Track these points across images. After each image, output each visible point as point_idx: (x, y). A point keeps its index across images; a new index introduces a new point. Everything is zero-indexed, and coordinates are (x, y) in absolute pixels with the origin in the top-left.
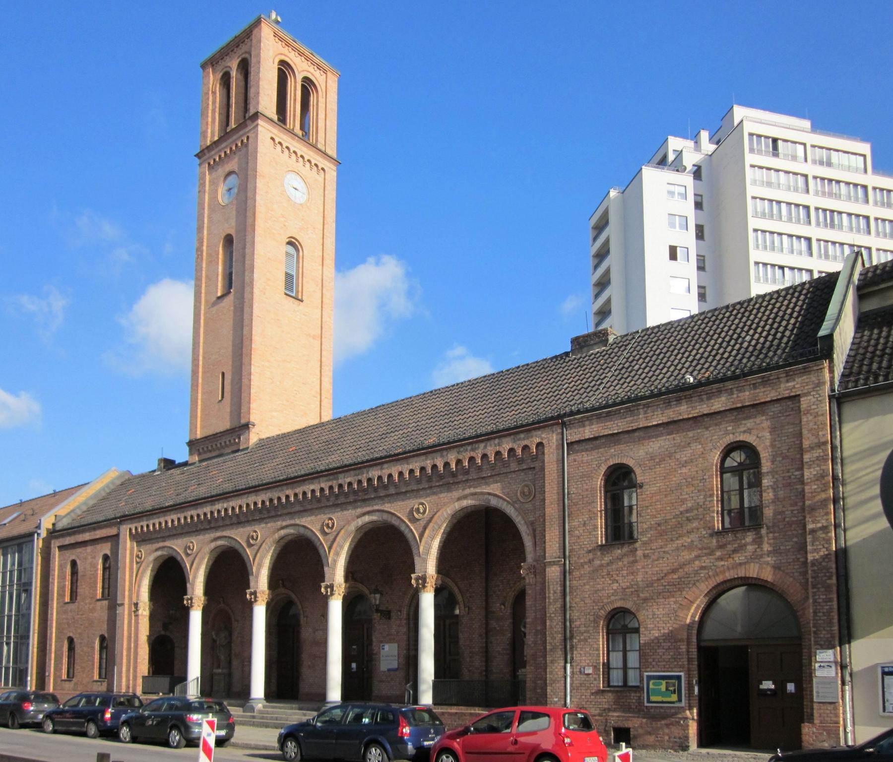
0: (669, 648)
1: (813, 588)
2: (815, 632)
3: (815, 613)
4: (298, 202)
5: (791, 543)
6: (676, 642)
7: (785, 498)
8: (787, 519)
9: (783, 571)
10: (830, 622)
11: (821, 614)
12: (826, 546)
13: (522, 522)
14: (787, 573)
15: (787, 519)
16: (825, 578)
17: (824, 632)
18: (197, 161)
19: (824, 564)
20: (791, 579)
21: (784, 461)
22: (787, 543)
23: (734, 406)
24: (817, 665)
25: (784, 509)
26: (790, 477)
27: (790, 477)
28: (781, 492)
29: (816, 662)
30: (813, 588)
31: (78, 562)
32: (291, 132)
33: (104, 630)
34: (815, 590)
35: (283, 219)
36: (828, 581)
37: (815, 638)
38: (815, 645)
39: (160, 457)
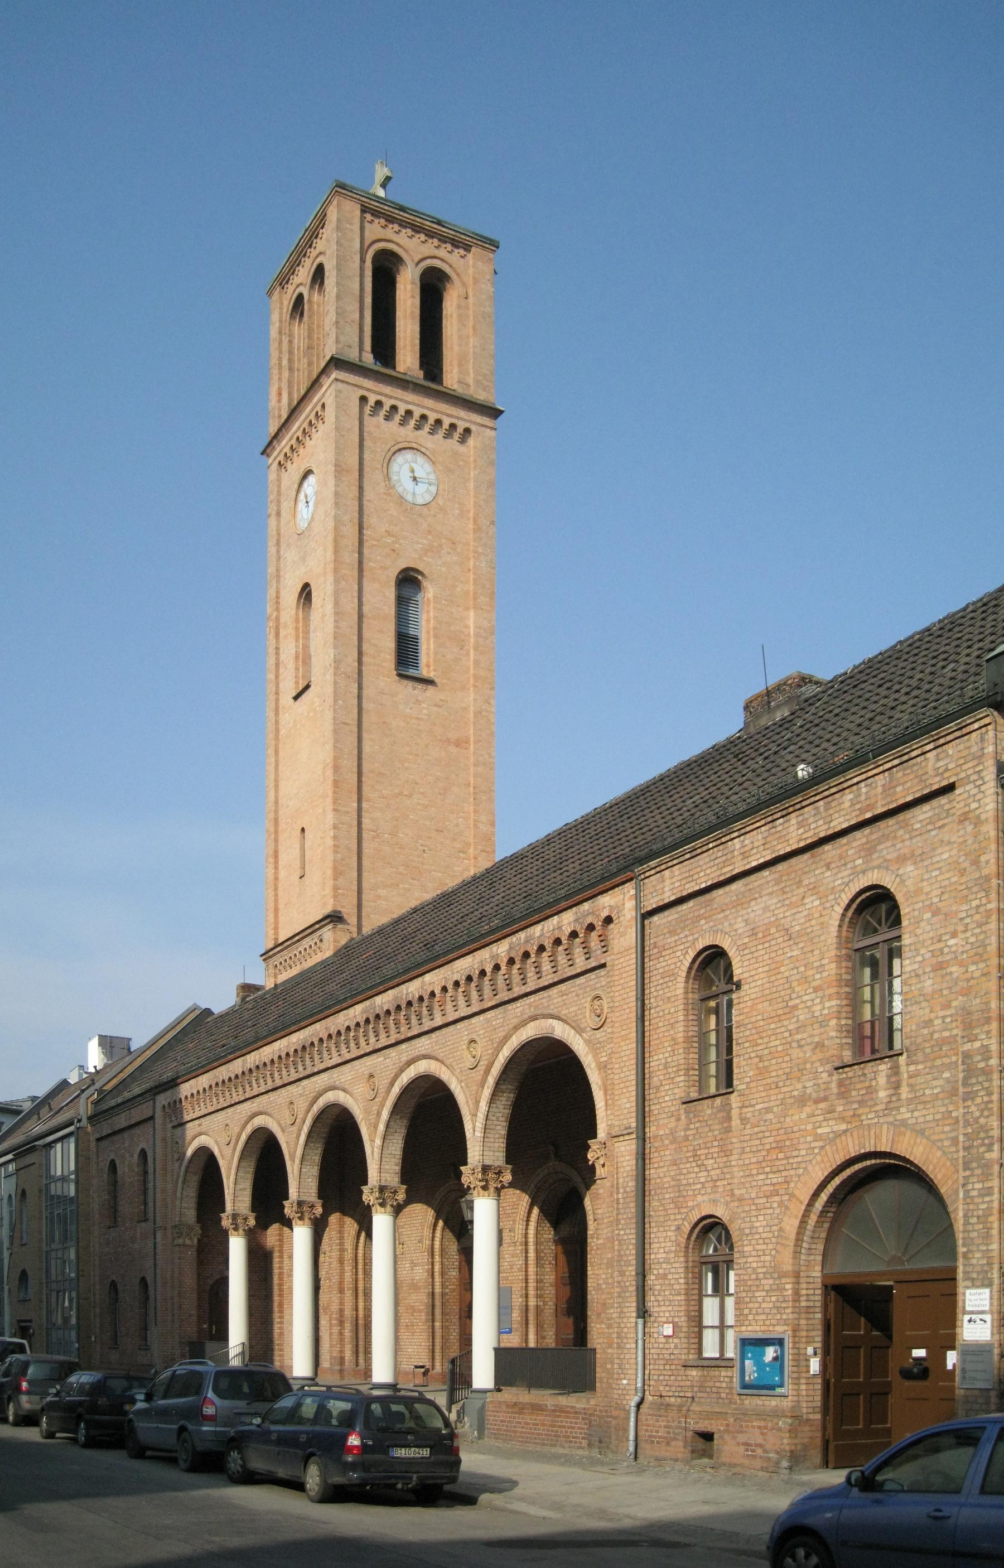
0: (771, 1290)
1: (964, 1170)
2: (965, 1255)
3: (965, 1216)
4: (420, 501)
5: (941, 1082)
6: (779, 1278)
7: (934, 992)
8: (936, 1036)
9: (928, 1138)
10: (987, 1236)
11: (974, 1220)
12: (986, 1085)
13: (593, 1065)
14: (934, 1142)
15: (936, 1036)
16: (982, 1149)
17: (977, 1255)
18: (264, 457)
19: (982, 1121)
20: (939, 1154)
21: (935, 919)
22: (935, 1083)
23: (861, 819)
24: (967, 1317)
25: (933, 1015)
26: (941, 950)
27: (941, 950)
28: (929, 982)
29: (965, 1312)
30: (964, 1170)
31: (117, 1162)
32: (404, 383)
33: (501, 1248)
34: (968, 1173)
35: (389, 540)
36: (987, 1155)
37: (964, 1265)
38: (965, 1280)
39: (241, 981)
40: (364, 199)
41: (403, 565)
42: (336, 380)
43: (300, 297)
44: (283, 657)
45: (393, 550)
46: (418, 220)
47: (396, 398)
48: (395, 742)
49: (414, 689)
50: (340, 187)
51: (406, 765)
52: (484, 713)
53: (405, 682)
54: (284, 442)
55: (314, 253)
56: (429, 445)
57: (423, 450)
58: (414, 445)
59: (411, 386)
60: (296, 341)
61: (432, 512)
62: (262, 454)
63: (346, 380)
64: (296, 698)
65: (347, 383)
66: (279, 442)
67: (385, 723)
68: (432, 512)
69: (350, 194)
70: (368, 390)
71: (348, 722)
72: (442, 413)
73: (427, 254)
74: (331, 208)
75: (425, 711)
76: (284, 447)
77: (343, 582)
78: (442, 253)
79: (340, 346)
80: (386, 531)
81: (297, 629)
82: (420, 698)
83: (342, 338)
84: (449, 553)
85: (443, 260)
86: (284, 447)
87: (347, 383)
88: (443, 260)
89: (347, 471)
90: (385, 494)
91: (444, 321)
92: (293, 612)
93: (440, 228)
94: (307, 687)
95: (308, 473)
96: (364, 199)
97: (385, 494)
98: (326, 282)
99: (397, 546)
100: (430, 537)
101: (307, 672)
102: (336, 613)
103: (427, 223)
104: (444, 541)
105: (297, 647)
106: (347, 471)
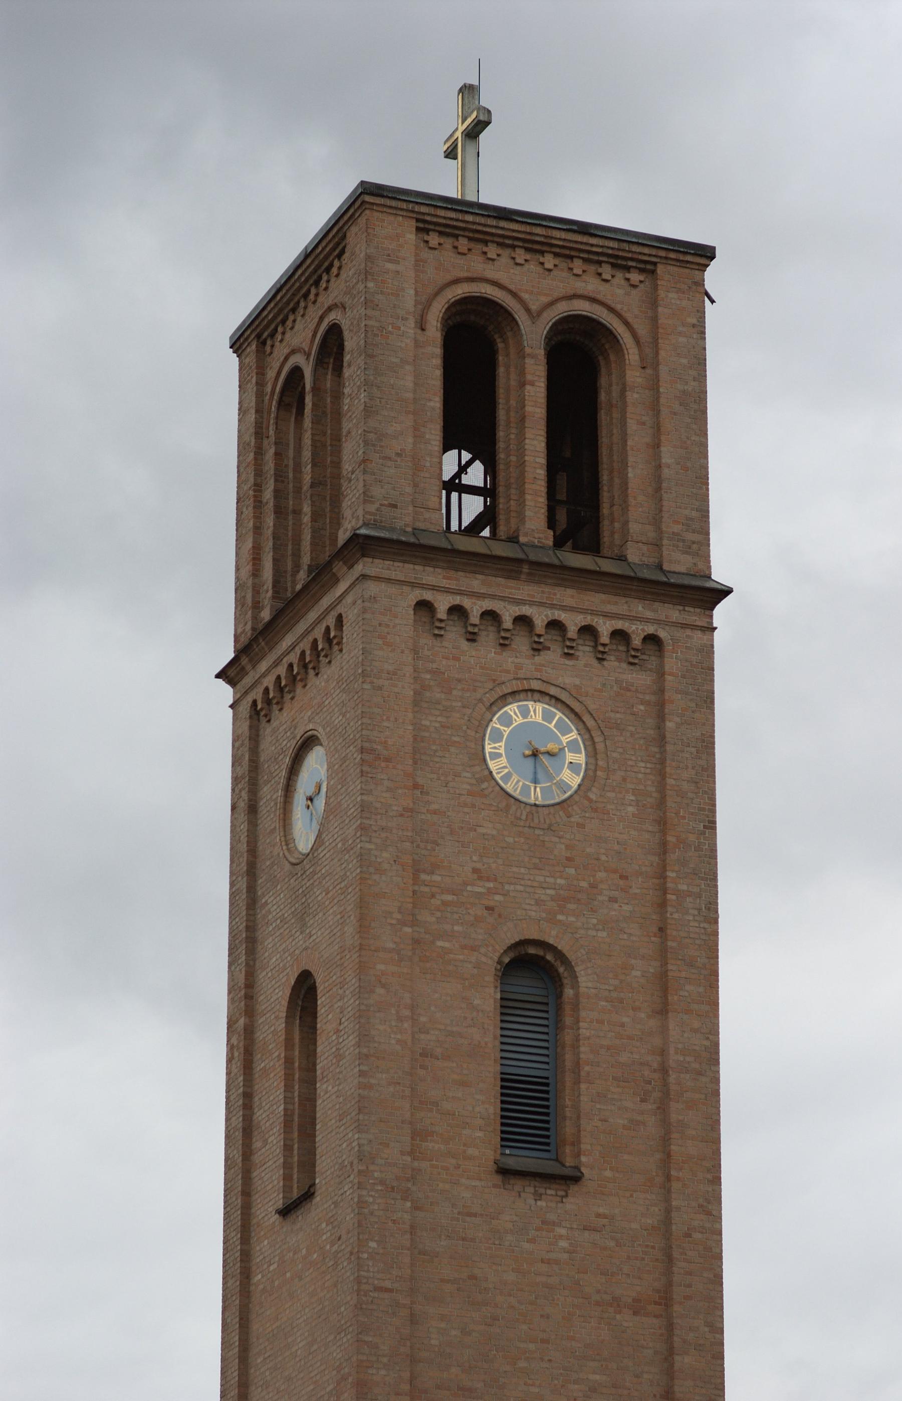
40: (424, 209)
41: (510, 935)
42: (364, 577)
43: (296, 372)
44: (259, 1115)
45: (489, 909)
46: (538, 230)
47: (493, 597)
48: (495, 1318)
49: (538, 1197)
50: (372, 194)
51: (522, 1364)
52: (697, 1236)
53: (518, 1184)
54: (263, 666)
55: (326, 300)
56: (568, 680)
57: (553, 691)
58: (536, 685)
59: (526, 569)
60: (291, 453)
61: (575, 819)
62: (218, 676)
63: (386, 574)
64: (286, 1212)
65: (389, 580)
66: (255, 664)
67: (473, 1277)
68: (575, 819)
69: (394, 203)
70: (433, 588)
71: (388, 1284)
72: (593, 613)
73: (556, 294)
74: (354, 229)
75: (563, 1244)
76: (264, 675)
77: (380, 991)
78: (591, 285)
79: (372, 508)
80: (475, 871)
81: (289, 1061)
82: (552, 1217)
83: (377, 492)
84: (613, 900)
85: (593, 300)
86: (264, 675)
87: (389, 580)
88: (593, 300)
89: (388, 760)
90: (470, 793)
91: (603, 417)
92: (281, 1025)
93: (585, 239)
94: (308, 1195)
95: (308, 743)
96: (424, 209)
97: (470, 793)
98: (347, 372)
99: (498, 898)
100: (572, 871)
101: (308, 1164)
102: (363, 1058)
103: (557, 234)
104: (601, 875)
105: (287, 1100)
106: (388, 760)
